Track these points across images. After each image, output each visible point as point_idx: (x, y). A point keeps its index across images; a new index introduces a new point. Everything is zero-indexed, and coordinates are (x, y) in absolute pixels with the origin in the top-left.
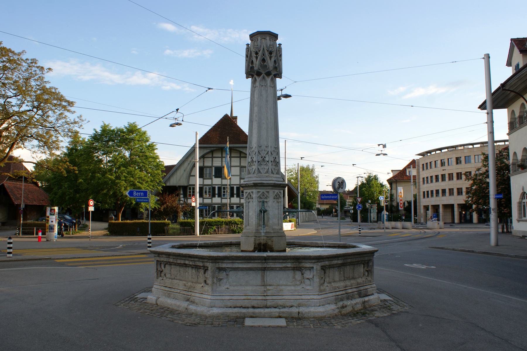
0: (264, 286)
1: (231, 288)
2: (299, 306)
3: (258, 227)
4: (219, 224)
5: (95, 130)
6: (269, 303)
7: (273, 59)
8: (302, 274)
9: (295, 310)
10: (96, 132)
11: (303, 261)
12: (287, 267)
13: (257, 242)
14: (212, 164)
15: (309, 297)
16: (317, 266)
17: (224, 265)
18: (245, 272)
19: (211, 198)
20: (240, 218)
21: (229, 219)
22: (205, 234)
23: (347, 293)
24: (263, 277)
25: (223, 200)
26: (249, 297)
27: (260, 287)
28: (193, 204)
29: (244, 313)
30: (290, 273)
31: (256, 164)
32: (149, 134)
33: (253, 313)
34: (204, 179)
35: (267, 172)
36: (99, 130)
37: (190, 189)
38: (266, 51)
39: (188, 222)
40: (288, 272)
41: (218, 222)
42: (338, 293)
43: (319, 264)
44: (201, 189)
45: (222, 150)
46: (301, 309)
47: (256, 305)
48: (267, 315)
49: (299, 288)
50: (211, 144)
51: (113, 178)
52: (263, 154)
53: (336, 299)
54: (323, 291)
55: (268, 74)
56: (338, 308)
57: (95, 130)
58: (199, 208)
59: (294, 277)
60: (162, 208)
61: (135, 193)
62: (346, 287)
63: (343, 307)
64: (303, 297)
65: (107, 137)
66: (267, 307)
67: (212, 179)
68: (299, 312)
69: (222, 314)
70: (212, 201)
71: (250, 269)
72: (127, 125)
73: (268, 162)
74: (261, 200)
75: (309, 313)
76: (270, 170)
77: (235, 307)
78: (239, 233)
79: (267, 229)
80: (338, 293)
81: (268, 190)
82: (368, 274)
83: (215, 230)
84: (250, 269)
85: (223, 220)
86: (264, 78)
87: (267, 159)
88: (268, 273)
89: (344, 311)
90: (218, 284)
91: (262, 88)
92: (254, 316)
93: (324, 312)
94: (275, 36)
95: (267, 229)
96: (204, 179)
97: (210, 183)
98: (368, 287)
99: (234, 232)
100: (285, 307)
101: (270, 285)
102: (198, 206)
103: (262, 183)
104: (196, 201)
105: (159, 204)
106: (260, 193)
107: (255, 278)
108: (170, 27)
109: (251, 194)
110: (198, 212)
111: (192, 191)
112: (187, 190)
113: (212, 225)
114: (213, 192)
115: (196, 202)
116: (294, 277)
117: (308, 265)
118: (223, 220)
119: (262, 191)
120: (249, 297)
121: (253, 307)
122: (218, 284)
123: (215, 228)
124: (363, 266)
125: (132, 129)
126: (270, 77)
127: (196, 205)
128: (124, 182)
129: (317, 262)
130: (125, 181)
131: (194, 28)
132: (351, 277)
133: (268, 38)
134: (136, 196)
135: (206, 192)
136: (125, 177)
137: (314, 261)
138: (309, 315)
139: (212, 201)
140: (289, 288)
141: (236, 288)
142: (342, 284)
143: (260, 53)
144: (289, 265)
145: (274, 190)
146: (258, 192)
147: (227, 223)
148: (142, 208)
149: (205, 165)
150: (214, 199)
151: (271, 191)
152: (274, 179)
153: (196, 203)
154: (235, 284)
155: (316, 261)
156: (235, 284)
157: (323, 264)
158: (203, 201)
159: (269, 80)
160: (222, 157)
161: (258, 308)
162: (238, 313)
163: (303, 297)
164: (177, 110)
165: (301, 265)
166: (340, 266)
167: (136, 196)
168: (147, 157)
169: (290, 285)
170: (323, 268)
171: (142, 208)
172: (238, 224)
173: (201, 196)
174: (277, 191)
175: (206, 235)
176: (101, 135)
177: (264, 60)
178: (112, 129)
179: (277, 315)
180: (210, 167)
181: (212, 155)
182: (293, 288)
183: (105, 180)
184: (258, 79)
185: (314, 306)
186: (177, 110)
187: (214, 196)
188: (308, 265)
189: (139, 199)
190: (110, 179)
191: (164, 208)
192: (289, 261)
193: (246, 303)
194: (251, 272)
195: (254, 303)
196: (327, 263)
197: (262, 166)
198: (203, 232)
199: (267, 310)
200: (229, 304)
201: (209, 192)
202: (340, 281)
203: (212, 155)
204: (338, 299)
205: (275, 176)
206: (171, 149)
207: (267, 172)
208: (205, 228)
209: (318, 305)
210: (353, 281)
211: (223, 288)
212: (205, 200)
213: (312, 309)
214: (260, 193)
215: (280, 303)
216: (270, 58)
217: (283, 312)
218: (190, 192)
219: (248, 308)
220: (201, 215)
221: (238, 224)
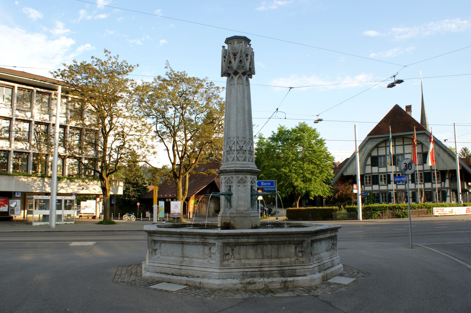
0: (183, 257)
1: (161, 257)
2: (203, 277)
3: (225, 208)
4: (382, 210)
5: (273, 132)
6: (183, 272)
7: (237, 60)
8: (210, 249)
9: (198, 280)
10: (274, 134)
11: (207, 237)
12: (197, 242)
13: (223, 222)
14: (378, 154)
15: (211, 270)
16: (219, 243)
17: (156, 238)
18: (171, 245)
19: (372, 186)
20: (416, 203)
21: (393, 204)
22: (369, 219)
23: (260, 271)
24: (182, 250)
25: (398, 186)
26: (171, 266)
27: (179, 258)
28: (355, 191)
29: (164, 278)
30: (201, 248)
31: (235, 152)
32: (318, 131)
33: (170, 279)
34: (379, 168)
35: (244, 160)
36: (276, 132)
37: (366, 177)
38: (243, 54)
39: (353, 208)
40: (199, 246)
41: (382, 207)
42: (246, 270)
43: (221, 241)
44: (362, 176)
45: (386, 141)
46: (205, 281)
47: (174, 273)
48: (178, 282)
49: (206, 261)
50: (382, 134)
51: (287, 171)
52: (231, 144)
53: (243, 275)
54: (227, 266)
55: (244, 74)
56: (241, 283)
57: (273, 132)
58: (361, 194)
59: (204, 252)
60: (337, 195)
61: (262, 183)
62: (261, 265)
63: (249, 283)
64: (207, 270)
65: (282, 136)
66: (181, 276)
67: (386, 167)
68: (200, 282)
69: (151, 277)
70: (387, 187)
71: (173, 242)
72: (298, 125)
73: (245, 151)
74: (229, 185)
75: (207, 283)
76: (235, 158)
77: (161, 273)
78: (403, 217)
79: (233, 210)
80: (246, 270)
81: (232, 176)
82: (303, 254)
83: (379, 215)
84: (173, 242)
85: (387, 205)
86: (240, 77)
87: (233, 149)
88: (185, 246)
89: (250, 287)
90: (154, 254)
91: (232, 86)
92: (170, 281)
93: (219, 285)
94: (247, 41)
95: (233, 210)
96: (379, 168)
97: (385, 171)
98: (297, 267)
99: (398, 217)
100: (193, 277)
101: (187, 257)
102: (360, 193)
103: (225, 170)
104: (357, 189)
105: (333, 192)
106: (227, 179)
107: (176, 249)
108: (372, 33)
109: (231, 179)
110: (360, 198)
111: (368, 179)
112: (353, 180)
113: (376, 211)
114: (375, 179)
115: (357, 189)
116: (204, 252)
117: (211, 241)
118: (387, 205)
119: (228, 177)
120: (171, 266)
121: (173, 275)
122: (154, 254)
123: (378, 213)
124: (294, 246)
125: (303, 129)
126: (238, 76)
127: (358, 192)
128: (294, 174)
129: (218, 239)
130: (295, 173)
131: (394, 29)
132: (273, 256)
133: (243, 42)
134: (264, 186)
135: (381, 179)
136: (296, 170)
137: (215, 238)
138: (208, 286)
139: (387, 187)
140: (199, 260)
141: (164, 257)
142: (257, 262)
143: (238, 56)
144: (198, 240)
145: (238, 176)
146: (226, 178)
147: (390, 208)
148: (312, 196)
149: (379, 154)
150: (389, 185)
151: (235, 177)
152: (238, 166)
153: (358, 190)
154: (164, 254)
155: (217, 238)
156: (164, 254)
157: (226, 241)
158: (379, 188)
159: (244, 78)
160: (403, 145)
161: (176, 275)
162: (160, 277)
163: (207, 270)
164: (277, 109)
165: (206, 241)
166: (255, 244)
167: (264, 186)
168: (314, 152)
169: (200, 258)
170: (226, 245)
171: (312, 196)
172: (402, 209)
173: (362, 184)
174: (241, 176)
175: (370, 220)
176: (278, 135)
177: (241, 61)
178: (287, 129)
179: (185, 283)
180: (385, 156)
181: (386, 144)
182: (201, 261)
183: (280, 173)
184: (236, 78)
185: (215, 279)
186: (277, 109)
187: (389, 182)
188: (211, 241)
189: (267, 188)
190: (284, 173)
191: (339, 196)
192: (197, 237)
193: (168, 271)
194: (175, 245)
195: (173, 271)
196: (232, 240)
197: (231, 155)
198: (365, 217)
199: (180, 278)
200: (158, 270)
201: (385, 179)
202: (256, 258)
203: (386, 144)
204: (244, 275)
205: (241, 162)
206: (342, 143)
207: (233, 160)
208: (368, 214)
209: (218, 278)
210: (275, 261)
211: (156, 257)
212: (381, 187)
213: (211, 281)
214: (227, 179)
215: (190, 273)
216: (235, 59)
217: (189, 281)
218: (366, 180)
219: (169, 274)
220: (363, 201)
221: (402, 209)
